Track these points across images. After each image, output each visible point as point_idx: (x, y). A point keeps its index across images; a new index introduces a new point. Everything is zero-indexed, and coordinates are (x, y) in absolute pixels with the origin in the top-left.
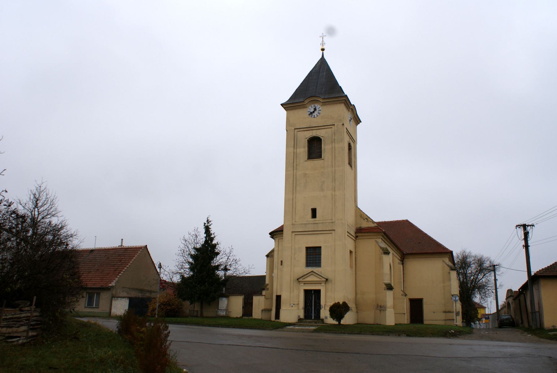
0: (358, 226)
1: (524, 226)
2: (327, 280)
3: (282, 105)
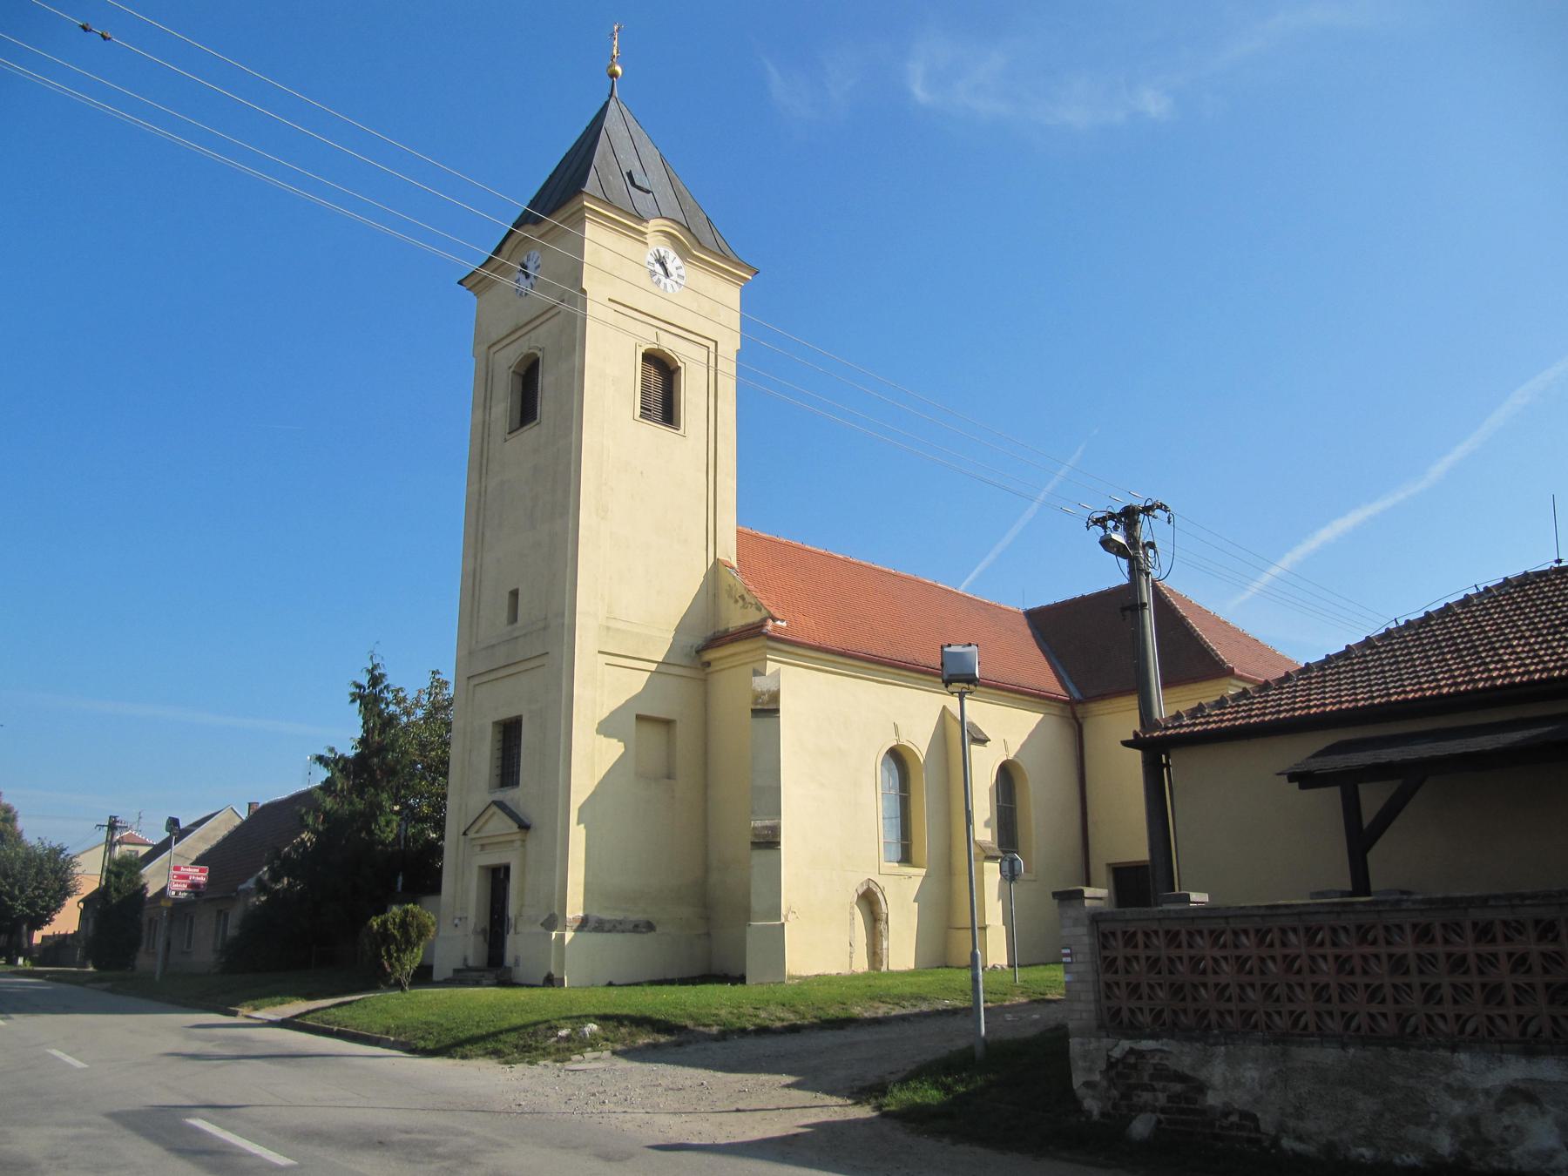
0: (722, 628)
1: (1129, 517)
2: (524, 827)
3: (460, 283)
